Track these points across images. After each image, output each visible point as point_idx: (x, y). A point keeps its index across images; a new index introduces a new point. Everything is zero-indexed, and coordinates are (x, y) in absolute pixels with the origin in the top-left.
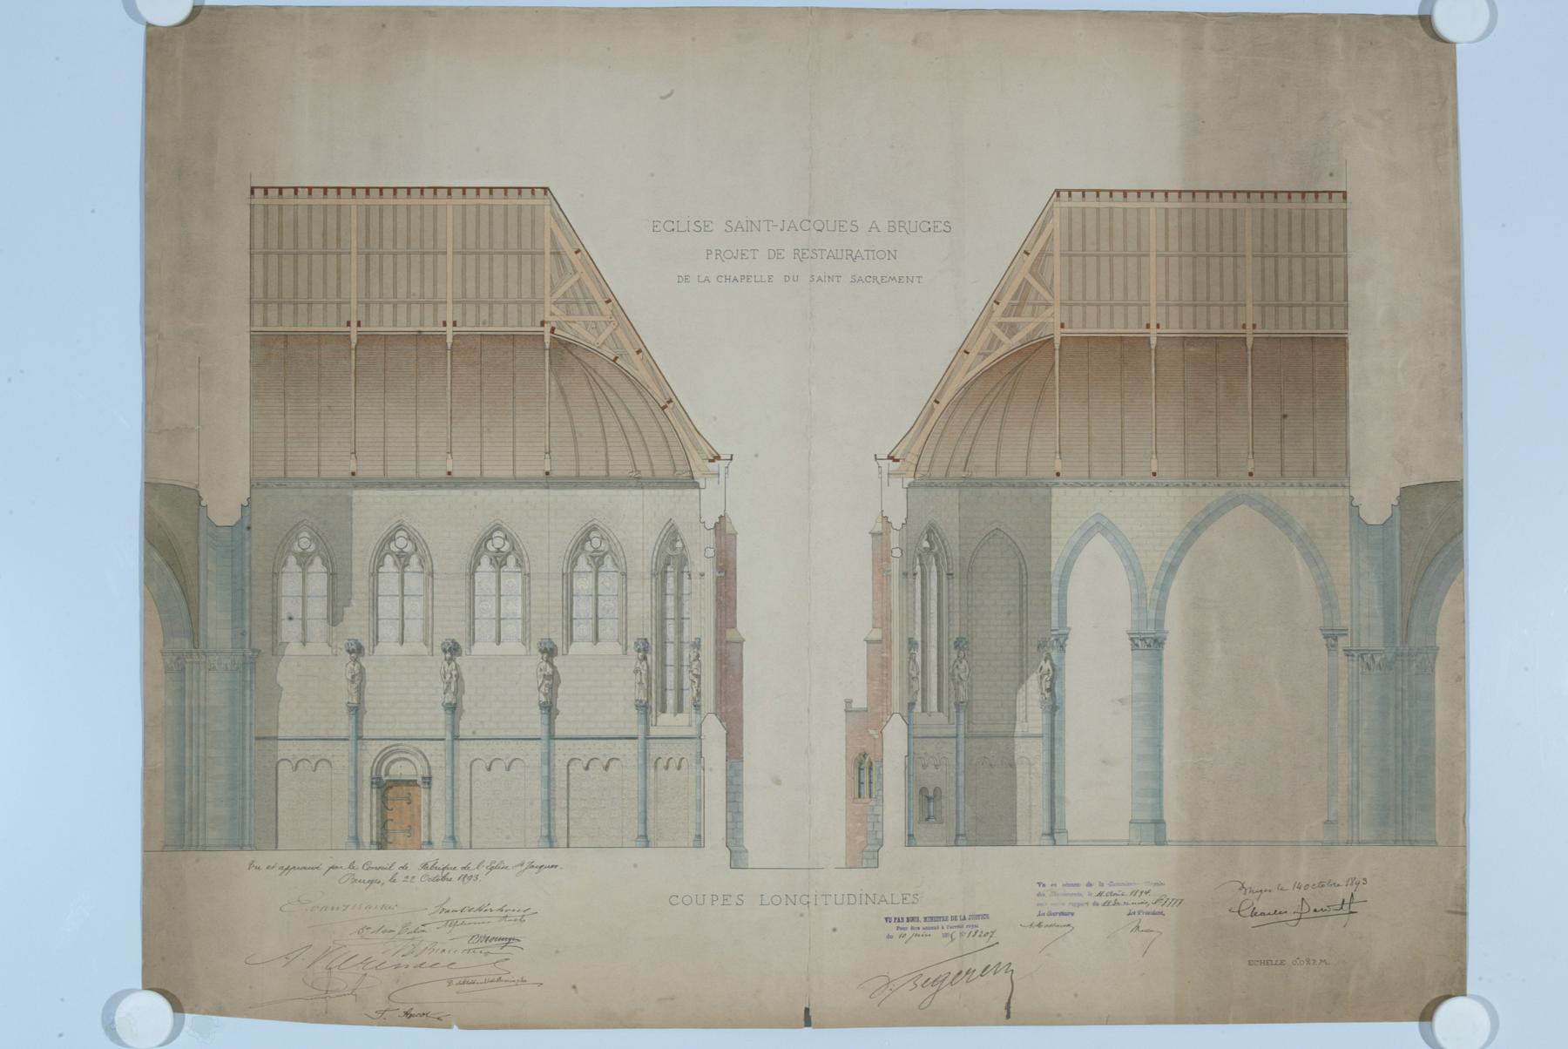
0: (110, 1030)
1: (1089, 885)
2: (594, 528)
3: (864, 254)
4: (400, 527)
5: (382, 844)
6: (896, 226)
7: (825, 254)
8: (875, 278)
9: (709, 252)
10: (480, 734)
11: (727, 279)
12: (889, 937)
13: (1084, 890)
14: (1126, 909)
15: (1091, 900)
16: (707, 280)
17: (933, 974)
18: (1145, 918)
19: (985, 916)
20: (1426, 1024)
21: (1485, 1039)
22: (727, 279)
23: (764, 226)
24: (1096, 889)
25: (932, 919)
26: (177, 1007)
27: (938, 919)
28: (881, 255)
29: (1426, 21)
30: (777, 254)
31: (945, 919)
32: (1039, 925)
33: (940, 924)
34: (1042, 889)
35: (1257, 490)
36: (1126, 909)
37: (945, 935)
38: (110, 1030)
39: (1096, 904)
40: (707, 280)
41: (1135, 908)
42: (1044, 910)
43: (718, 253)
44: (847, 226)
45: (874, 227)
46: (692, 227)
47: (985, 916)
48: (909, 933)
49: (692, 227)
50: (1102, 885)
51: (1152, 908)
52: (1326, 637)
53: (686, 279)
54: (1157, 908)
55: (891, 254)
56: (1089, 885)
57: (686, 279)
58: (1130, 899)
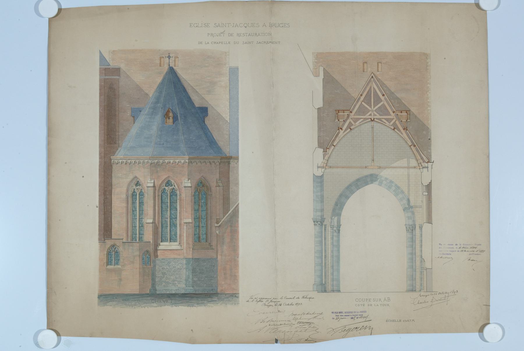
0: (37, 344)
1: (456, 245)
3: (261, 34)
5: (171, 242)
7: (248, 35)
9: (208, 34)
13: (455, 246)
15: (457, 250)
16: (208, 43)
17: (347, 328)
20: (481, 333)
21: (501, 337)
24: (458, 246)
26: (58, 334)
29: (478, 5)
31: (352, 312)
33: (350, 314)
37: (352, 318)
38: (37, 344)
39: (458, 251)
40: (208, 43)
41: (471, 253)
43: (212, 34)
44: (242, 35)
46: (203, 25)
47: (365, 312)
49: (203, 25)
50: (460, 245)
52: (314, 222)
56: (456, 245)
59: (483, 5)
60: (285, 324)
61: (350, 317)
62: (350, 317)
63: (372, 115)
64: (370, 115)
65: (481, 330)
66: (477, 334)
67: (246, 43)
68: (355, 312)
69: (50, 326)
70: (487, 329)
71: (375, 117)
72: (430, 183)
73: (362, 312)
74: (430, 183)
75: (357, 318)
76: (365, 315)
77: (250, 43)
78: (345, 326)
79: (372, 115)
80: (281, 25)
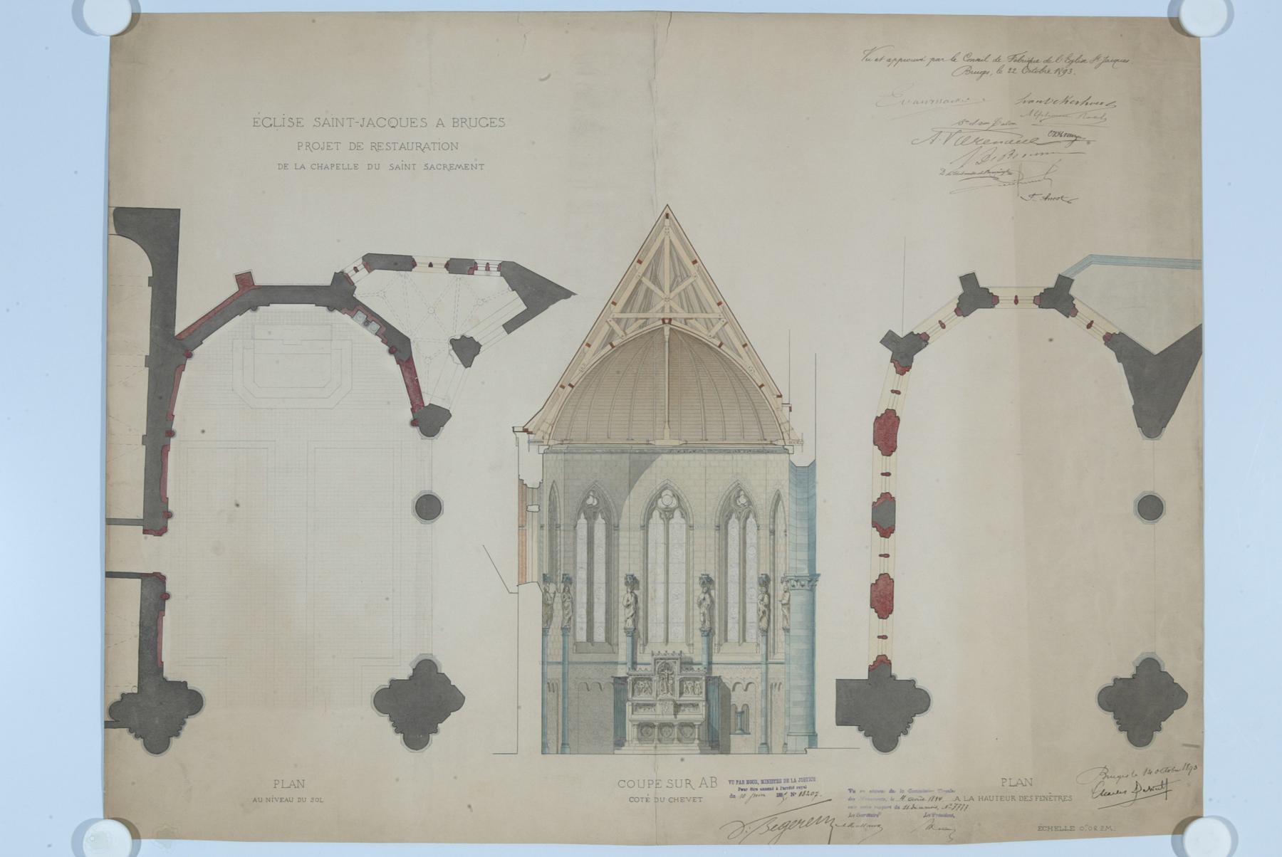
1: (892, 791)
2: (665, 488)
3: (431, 146)
4: (665, 488)
6: (458, 122)
7: (398, 147)
8: (445, 166)
10: (803, 539)
11: (320, 167)
12: (732, 796)
13: (888, 795)
14: (923, 812)
15: (893, 804)
17: (780, 820)
18: (937, 819)
19: (813, 779)
22: (320, 167)
23: (347, 123)
25: (768, 781)
26: (135, 834)
27: (772, 781)
28: (445, 146)
30: (357, 146)
31: (779, 781)
32: (851, 825)
33: (774, 785)
34: (852, 795)
35: (560, 607)
36: (923, 812)
37: (780, 795)
42: (854, 812)
45: (440, 123)
47: (813, 779)
48: (749, 793)
51: (943, 812)
53: (285, 166)
54: (949, 812)
55: (453, 146)
56: (892, 791)
57: (285, 166)
58: (924, 804)
59: (1189, 23)
60: (914, 807)
61: (775, 792)
62: (775, 792)
63: (667, 309)
64: (663, 309)
65: (1180, 829)
66: (1167, 839)
67: (398, 167)
68: (787, 781)
69: (112, 812)
70: (1193, 829)
71: (672, 316)
72: (814, 463)
73: (804, 780)
74: (814, 463)
75: (793, 794)
76: (811, 787)
77: (407, 167)
78: (775, 816)
79: (667, 309)
80: (483, 122)
